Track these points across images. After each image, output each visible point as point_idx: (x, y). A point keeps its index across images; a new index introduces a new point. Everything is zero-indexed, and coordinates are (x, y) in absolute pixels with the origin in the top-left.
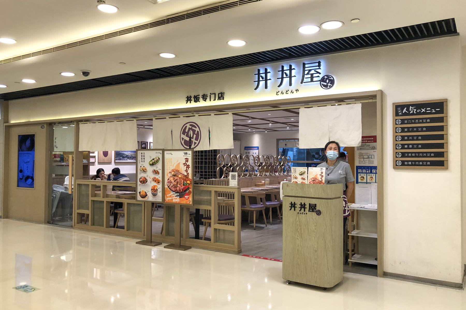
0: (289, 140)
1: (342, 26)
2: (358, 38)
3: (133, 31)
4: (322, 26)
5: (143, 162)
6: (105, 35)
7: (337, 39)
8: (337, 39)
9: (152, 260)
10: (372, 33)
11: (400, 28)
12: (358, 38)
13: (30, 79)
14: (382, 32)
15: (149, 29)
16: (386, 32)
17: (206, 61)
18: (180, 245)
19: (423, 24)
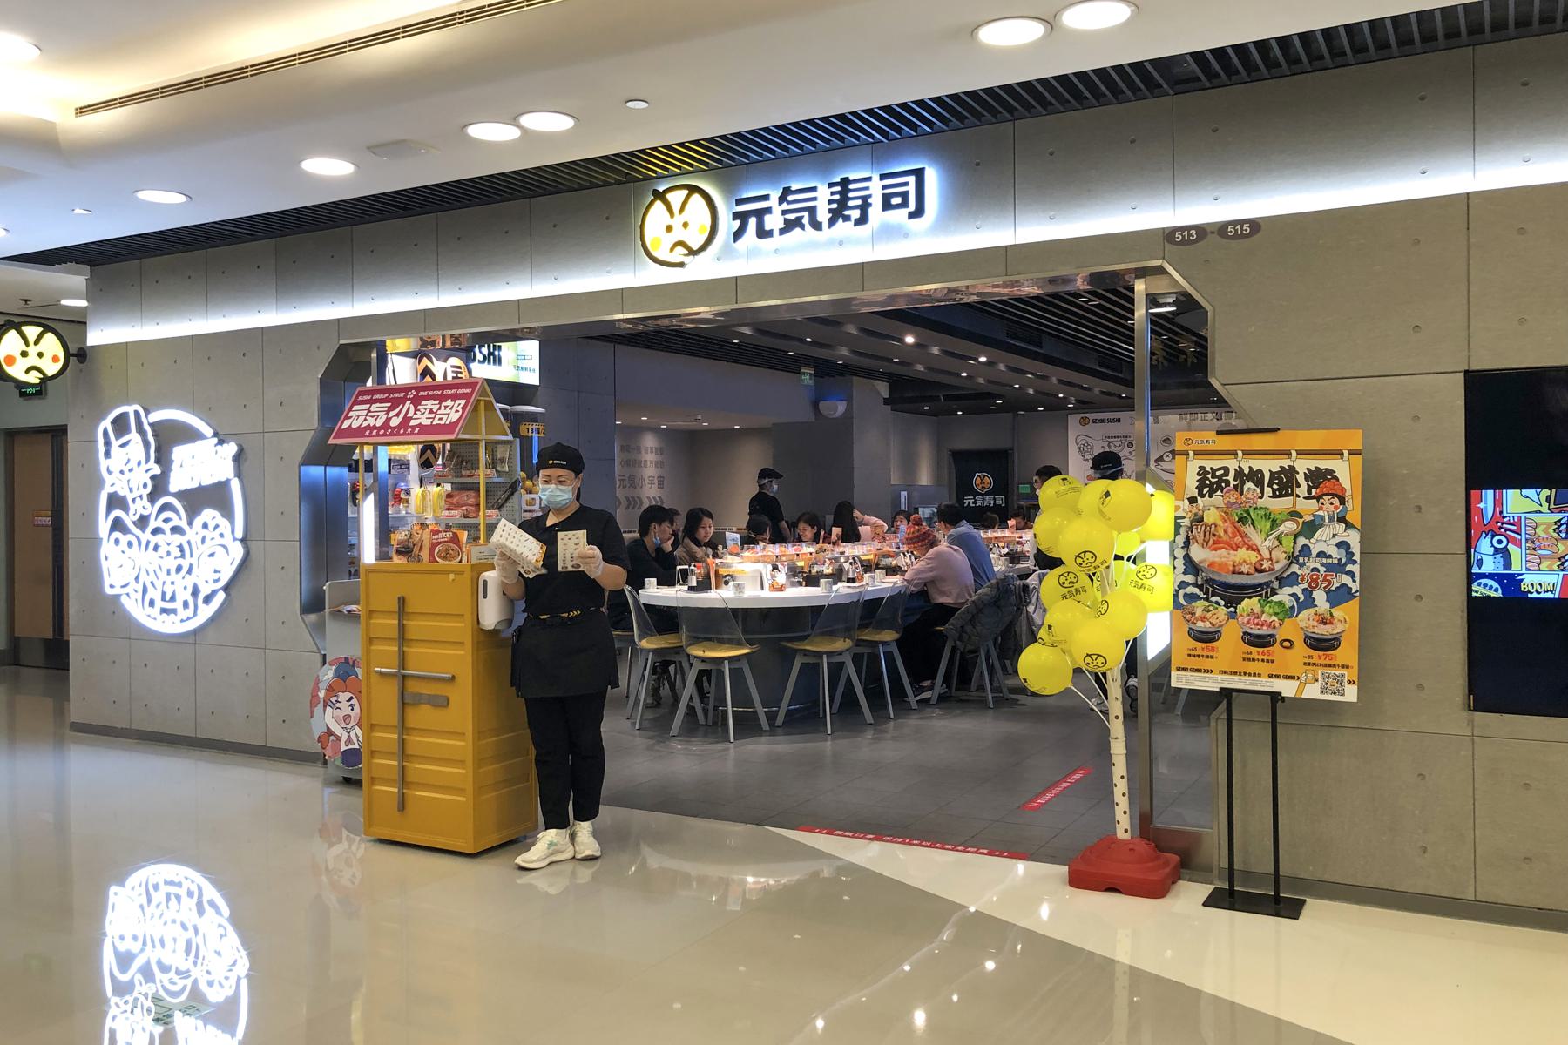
0: (443, 390)
1: (1043, 37)
2: (1058, 87)
3: (401, 35)
4: (977, 33)
5: (1107, 565)
6: (206, 77)
7: (1009, 86)
8: (974, 91)
9: (399, 670)
10: (1121, 65)
11: (1222, 50)
12: (1058, 87)
13: (315, 175)
14: (1145, 64)
15: (204, 89)
16: (1119, 69)
17: (618, 154)
18: (1277, 899)
19: (1255, 43)
